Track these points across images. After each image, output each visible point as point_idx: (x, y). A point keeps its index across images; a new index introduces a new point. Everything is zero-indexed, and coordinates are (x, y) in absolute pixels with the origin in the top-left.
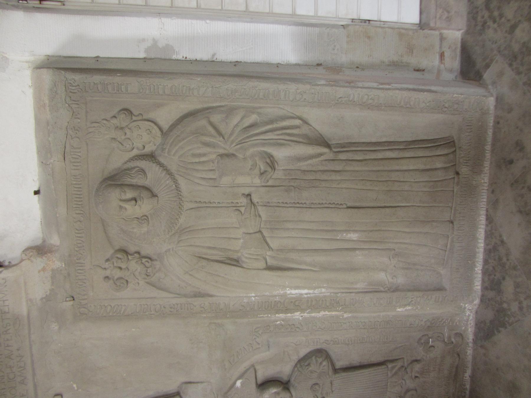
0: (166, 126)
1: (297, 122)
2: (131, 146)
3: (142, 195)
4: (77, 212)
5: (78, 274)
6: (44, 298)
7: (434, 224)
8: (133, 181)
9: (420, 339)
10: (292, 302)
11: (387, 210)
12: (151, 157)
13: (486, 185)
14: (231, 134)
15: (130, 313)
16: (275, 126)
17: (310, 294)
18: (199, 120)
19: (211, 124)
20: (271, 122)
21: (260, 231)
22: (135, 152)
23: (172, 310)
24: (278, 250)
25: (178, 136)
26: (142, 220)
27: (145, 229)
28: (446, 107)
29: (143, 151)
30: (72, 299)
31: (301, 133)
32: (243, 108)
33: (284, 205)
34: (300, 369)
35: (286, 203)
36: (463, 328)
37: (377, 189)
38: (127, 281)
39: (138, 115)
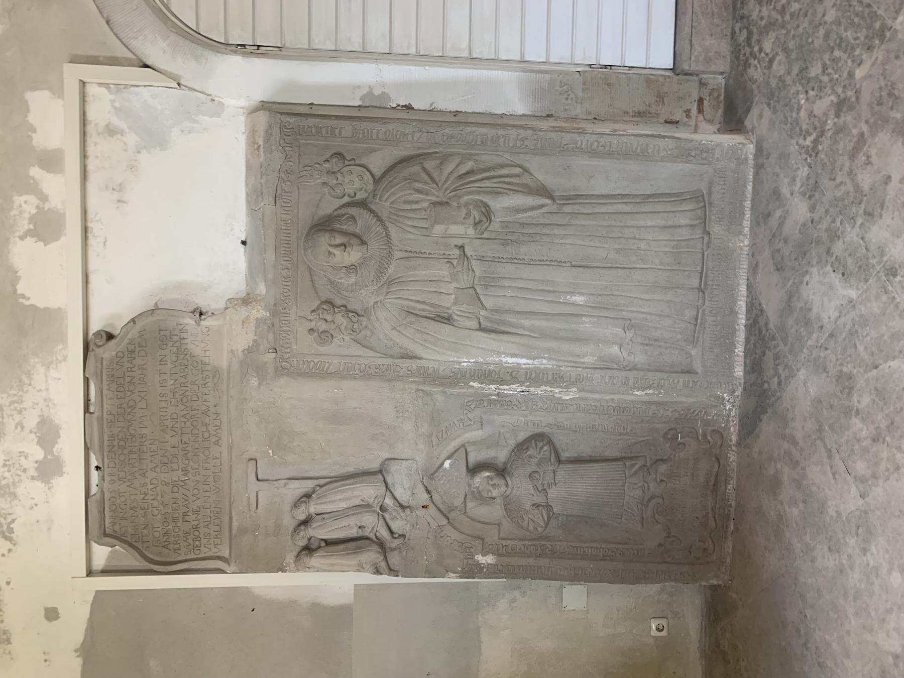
0: (378, 173)
1: (517, 171)
2: (343, 191)
3: (351, 242)
4: (285, 259)
5: (282, 325)
6: (246, 349)
7: (679, 291)
8: (343, 227)
9: (666, 434)
10: (508, 372)
11: (620, 271)
12: (363, 204)
13: (747, 248)
14: (446, 181)
15: (333, 371)
16: (492, 173)
17: (529, 364)
18: (412, 166)
19: (424, 170)
20: (488, 169)
21: (473, 287)
22: (346, 199)
23: (377, 371)
24: (492, 310)
25: (390, 182)
26: (351, 269)
27: (353, 280)
28: (692, 156)
29: (355, 198)
30: (275, 351)
31: (520, 182)
32: (459, 154)
33: (500, 260)
34: (517, 453)
35: (502, 258)
36: (723, 425)
37: (606, 246)
38: (332, 335)
39: (350, 160)
